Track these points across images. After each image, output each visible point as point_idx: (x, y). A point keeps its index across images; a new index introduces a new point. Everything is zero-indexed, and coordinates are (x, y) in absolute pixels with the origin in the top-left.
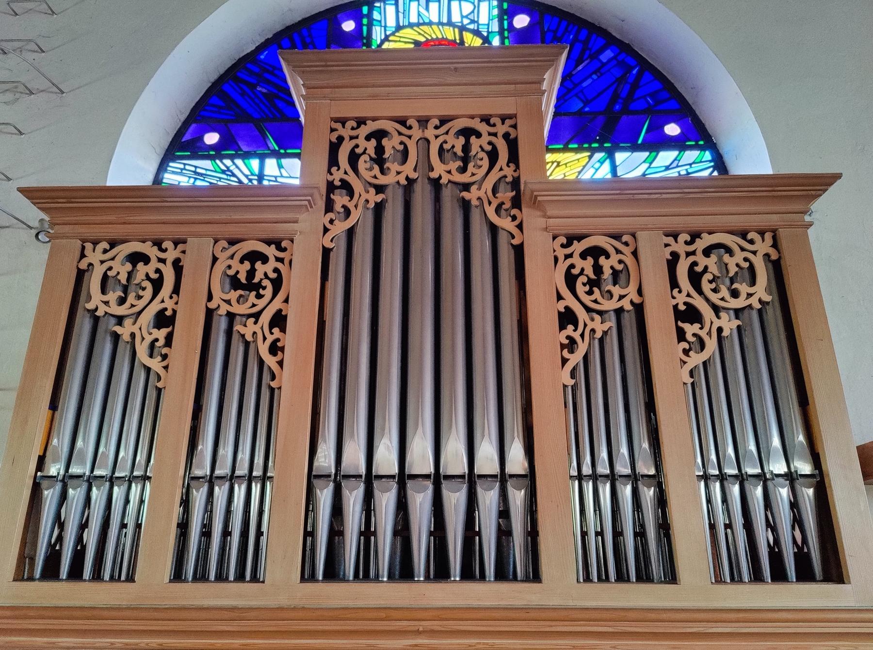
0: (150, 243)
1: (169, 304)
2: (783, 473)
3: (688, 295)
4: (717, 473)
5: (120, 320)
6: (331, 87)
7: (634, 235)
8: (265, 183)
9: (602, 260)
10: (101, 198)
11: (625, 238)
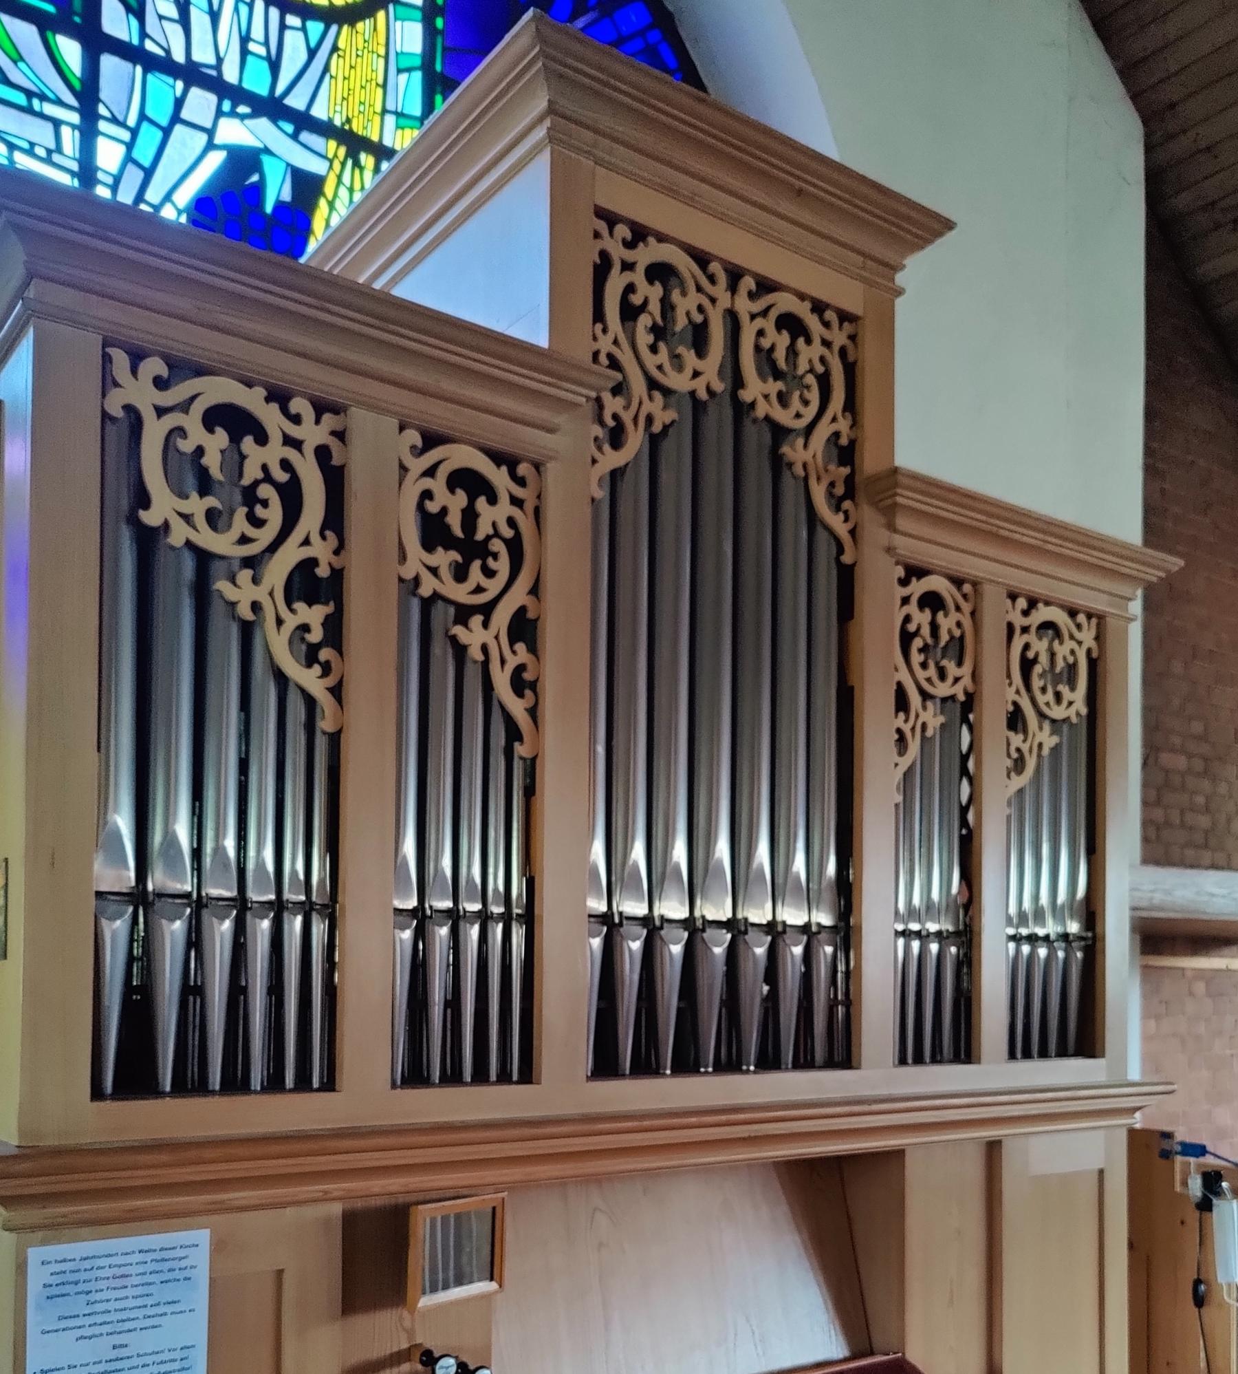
0: (260, 392)
1: (321, 550)
2: (724, 919)
3: (616, 342)
4: (303, 898)
5: (463, 614)
6: (596, 131)
7: (537, 466)
8: (143, 207)
9: (481, 503)
10: (345, 306)
11: (967, 588)
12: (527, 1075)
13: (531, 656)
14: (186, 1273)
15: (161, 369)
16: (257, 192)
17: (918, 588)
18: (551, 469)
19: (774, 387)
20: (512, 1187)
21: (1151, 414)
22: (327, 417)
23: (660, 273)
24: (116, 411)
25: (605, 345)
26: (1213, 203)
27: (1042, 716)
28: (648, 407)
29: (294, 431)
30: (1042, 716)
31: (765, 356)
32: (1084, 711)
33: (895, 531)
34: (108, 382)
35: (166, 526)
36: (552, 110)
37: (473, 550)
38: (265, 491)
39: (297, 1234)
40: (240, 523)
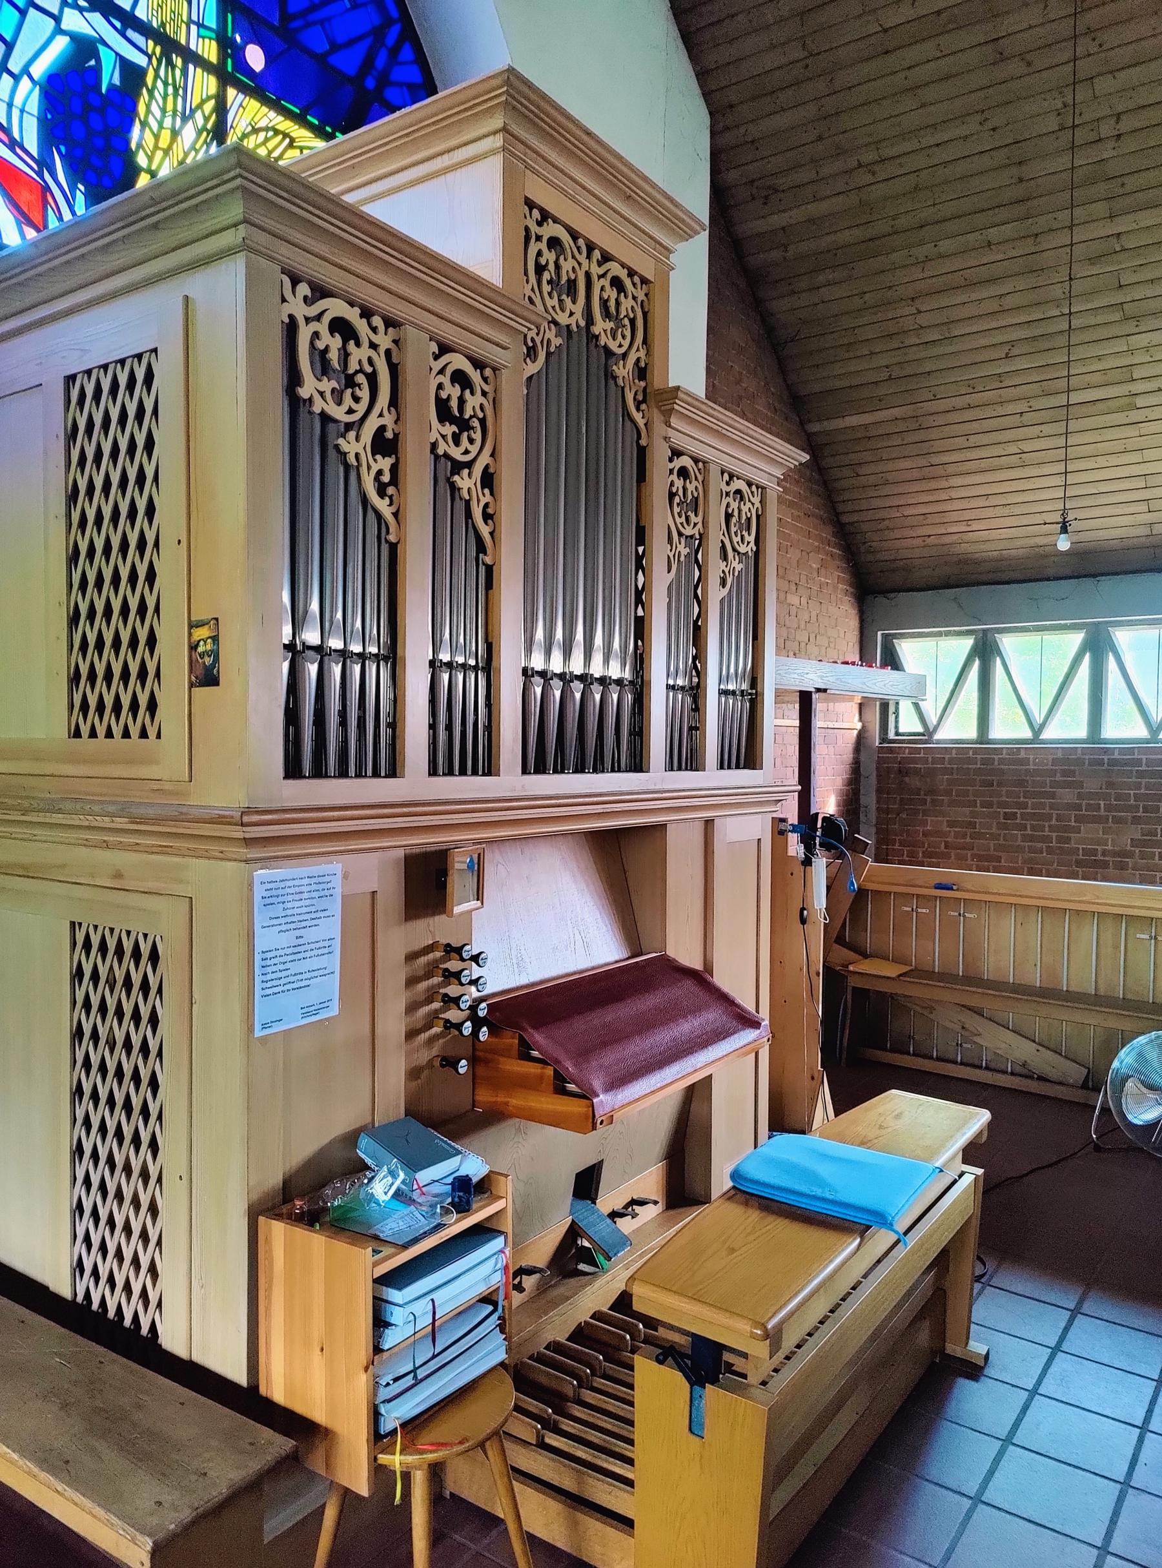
0: (357, 310)
7: (494, 369)
11: (701, 464)
12: (393, 773)
14: (331, 892)
16: (97, 71)
17: (678, 463)
18: (505, 374)
19: (610, 325)
20: (491, 842)
21: (710, 330)
23: (554, 243)
25: (528, 293)
26: (753, 181)
27: (734, 550)
29: (375, 339)
30: (734, 550)
31: (604, 303)
32: (754, 549)
33: (670, 426)
35: (310, 400)
36: (505, 129)
37: (464, 425)
39: (376, 870)
40: (348, 400)
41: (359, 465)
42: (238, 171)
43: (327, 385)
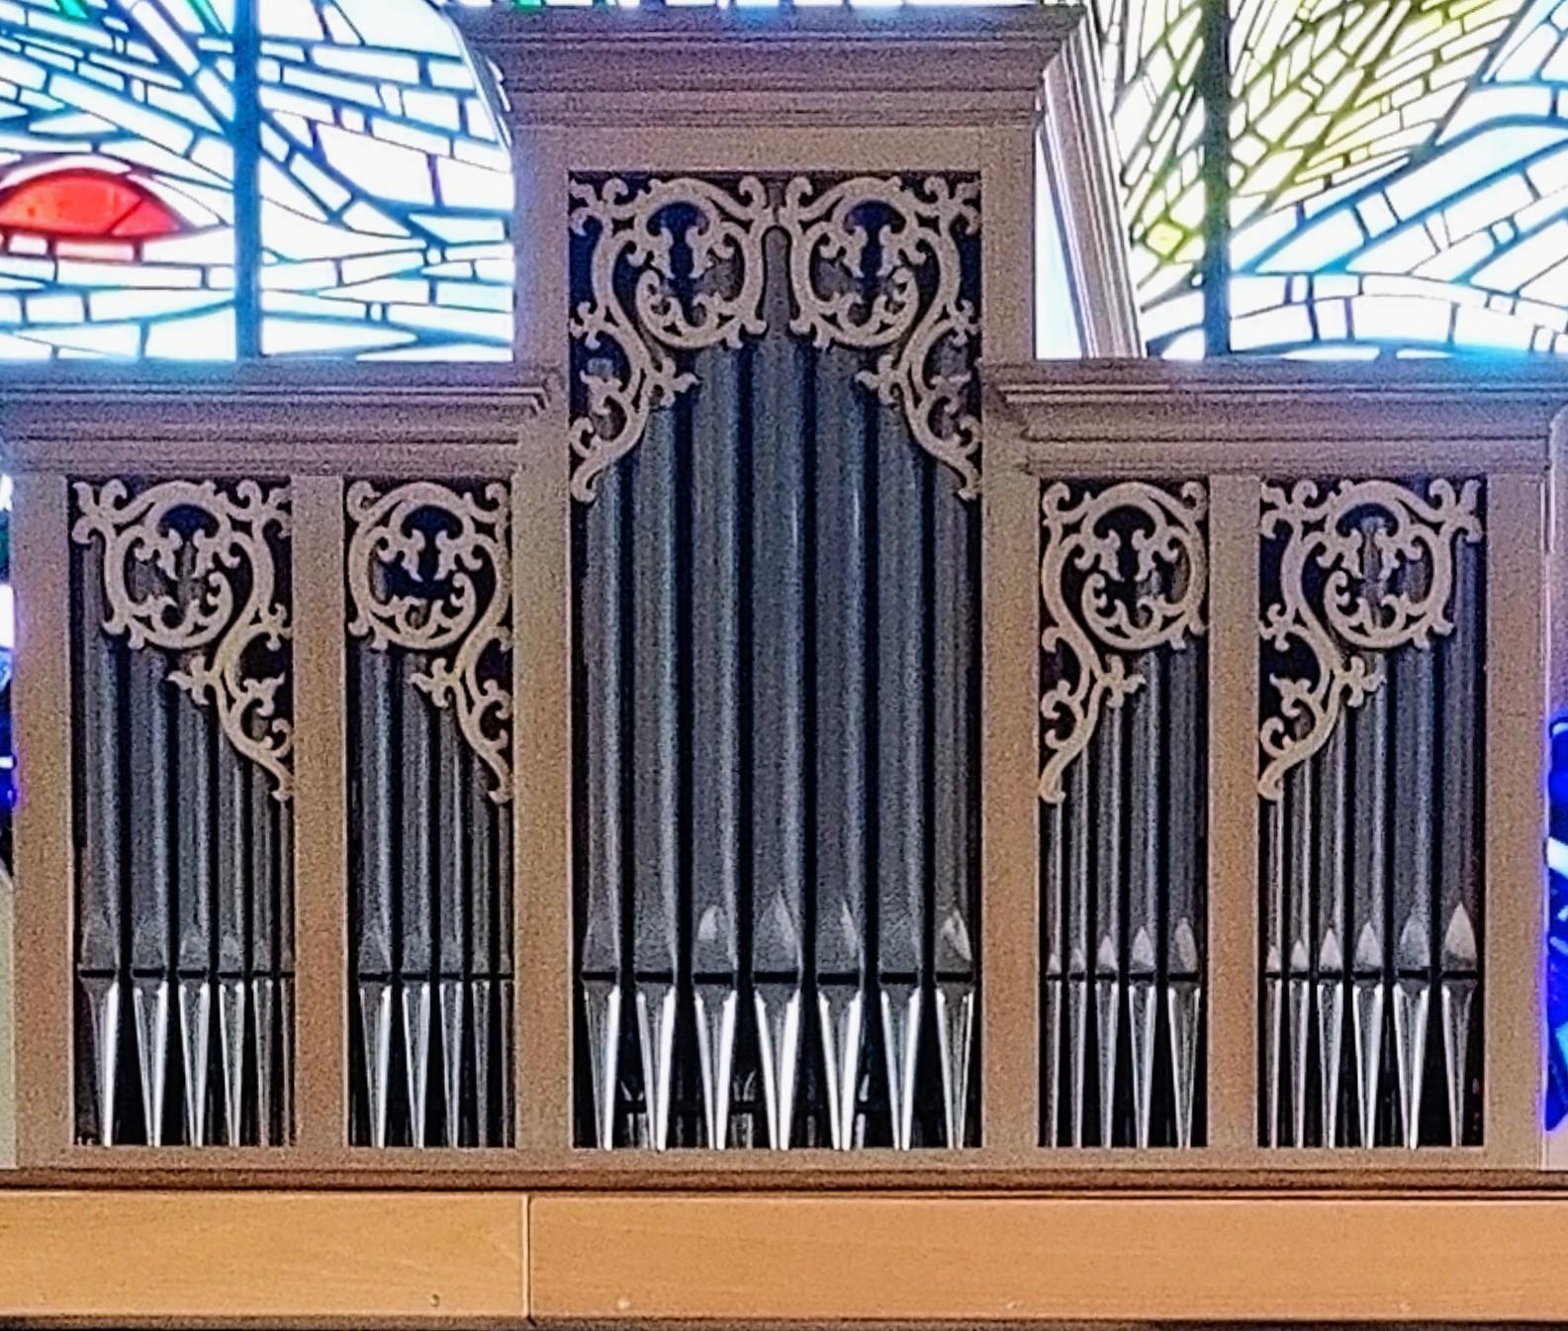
0: (209, 485)
1: (271, 625)
3: (609, 318)
13: (504, 693)
15: (116, 489)
22: (274, 493)
24: (81, 538)
28: (654, 377)
29: (241, 515)
34: (75, 513)
35: (127, 630)
38: (217, 578)
41: (453, 704)
42: (539, 390)
43: (398, 607)
